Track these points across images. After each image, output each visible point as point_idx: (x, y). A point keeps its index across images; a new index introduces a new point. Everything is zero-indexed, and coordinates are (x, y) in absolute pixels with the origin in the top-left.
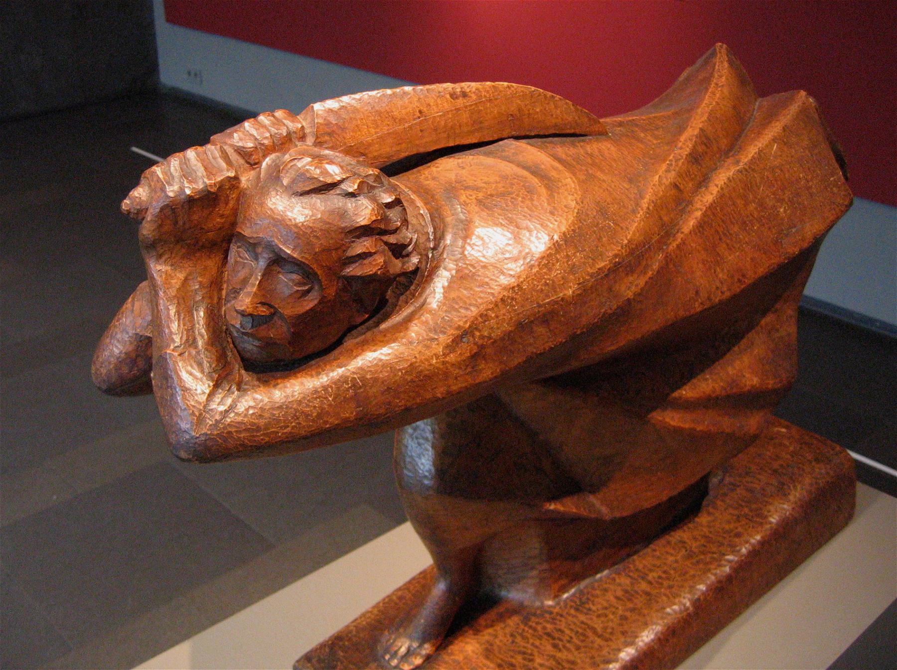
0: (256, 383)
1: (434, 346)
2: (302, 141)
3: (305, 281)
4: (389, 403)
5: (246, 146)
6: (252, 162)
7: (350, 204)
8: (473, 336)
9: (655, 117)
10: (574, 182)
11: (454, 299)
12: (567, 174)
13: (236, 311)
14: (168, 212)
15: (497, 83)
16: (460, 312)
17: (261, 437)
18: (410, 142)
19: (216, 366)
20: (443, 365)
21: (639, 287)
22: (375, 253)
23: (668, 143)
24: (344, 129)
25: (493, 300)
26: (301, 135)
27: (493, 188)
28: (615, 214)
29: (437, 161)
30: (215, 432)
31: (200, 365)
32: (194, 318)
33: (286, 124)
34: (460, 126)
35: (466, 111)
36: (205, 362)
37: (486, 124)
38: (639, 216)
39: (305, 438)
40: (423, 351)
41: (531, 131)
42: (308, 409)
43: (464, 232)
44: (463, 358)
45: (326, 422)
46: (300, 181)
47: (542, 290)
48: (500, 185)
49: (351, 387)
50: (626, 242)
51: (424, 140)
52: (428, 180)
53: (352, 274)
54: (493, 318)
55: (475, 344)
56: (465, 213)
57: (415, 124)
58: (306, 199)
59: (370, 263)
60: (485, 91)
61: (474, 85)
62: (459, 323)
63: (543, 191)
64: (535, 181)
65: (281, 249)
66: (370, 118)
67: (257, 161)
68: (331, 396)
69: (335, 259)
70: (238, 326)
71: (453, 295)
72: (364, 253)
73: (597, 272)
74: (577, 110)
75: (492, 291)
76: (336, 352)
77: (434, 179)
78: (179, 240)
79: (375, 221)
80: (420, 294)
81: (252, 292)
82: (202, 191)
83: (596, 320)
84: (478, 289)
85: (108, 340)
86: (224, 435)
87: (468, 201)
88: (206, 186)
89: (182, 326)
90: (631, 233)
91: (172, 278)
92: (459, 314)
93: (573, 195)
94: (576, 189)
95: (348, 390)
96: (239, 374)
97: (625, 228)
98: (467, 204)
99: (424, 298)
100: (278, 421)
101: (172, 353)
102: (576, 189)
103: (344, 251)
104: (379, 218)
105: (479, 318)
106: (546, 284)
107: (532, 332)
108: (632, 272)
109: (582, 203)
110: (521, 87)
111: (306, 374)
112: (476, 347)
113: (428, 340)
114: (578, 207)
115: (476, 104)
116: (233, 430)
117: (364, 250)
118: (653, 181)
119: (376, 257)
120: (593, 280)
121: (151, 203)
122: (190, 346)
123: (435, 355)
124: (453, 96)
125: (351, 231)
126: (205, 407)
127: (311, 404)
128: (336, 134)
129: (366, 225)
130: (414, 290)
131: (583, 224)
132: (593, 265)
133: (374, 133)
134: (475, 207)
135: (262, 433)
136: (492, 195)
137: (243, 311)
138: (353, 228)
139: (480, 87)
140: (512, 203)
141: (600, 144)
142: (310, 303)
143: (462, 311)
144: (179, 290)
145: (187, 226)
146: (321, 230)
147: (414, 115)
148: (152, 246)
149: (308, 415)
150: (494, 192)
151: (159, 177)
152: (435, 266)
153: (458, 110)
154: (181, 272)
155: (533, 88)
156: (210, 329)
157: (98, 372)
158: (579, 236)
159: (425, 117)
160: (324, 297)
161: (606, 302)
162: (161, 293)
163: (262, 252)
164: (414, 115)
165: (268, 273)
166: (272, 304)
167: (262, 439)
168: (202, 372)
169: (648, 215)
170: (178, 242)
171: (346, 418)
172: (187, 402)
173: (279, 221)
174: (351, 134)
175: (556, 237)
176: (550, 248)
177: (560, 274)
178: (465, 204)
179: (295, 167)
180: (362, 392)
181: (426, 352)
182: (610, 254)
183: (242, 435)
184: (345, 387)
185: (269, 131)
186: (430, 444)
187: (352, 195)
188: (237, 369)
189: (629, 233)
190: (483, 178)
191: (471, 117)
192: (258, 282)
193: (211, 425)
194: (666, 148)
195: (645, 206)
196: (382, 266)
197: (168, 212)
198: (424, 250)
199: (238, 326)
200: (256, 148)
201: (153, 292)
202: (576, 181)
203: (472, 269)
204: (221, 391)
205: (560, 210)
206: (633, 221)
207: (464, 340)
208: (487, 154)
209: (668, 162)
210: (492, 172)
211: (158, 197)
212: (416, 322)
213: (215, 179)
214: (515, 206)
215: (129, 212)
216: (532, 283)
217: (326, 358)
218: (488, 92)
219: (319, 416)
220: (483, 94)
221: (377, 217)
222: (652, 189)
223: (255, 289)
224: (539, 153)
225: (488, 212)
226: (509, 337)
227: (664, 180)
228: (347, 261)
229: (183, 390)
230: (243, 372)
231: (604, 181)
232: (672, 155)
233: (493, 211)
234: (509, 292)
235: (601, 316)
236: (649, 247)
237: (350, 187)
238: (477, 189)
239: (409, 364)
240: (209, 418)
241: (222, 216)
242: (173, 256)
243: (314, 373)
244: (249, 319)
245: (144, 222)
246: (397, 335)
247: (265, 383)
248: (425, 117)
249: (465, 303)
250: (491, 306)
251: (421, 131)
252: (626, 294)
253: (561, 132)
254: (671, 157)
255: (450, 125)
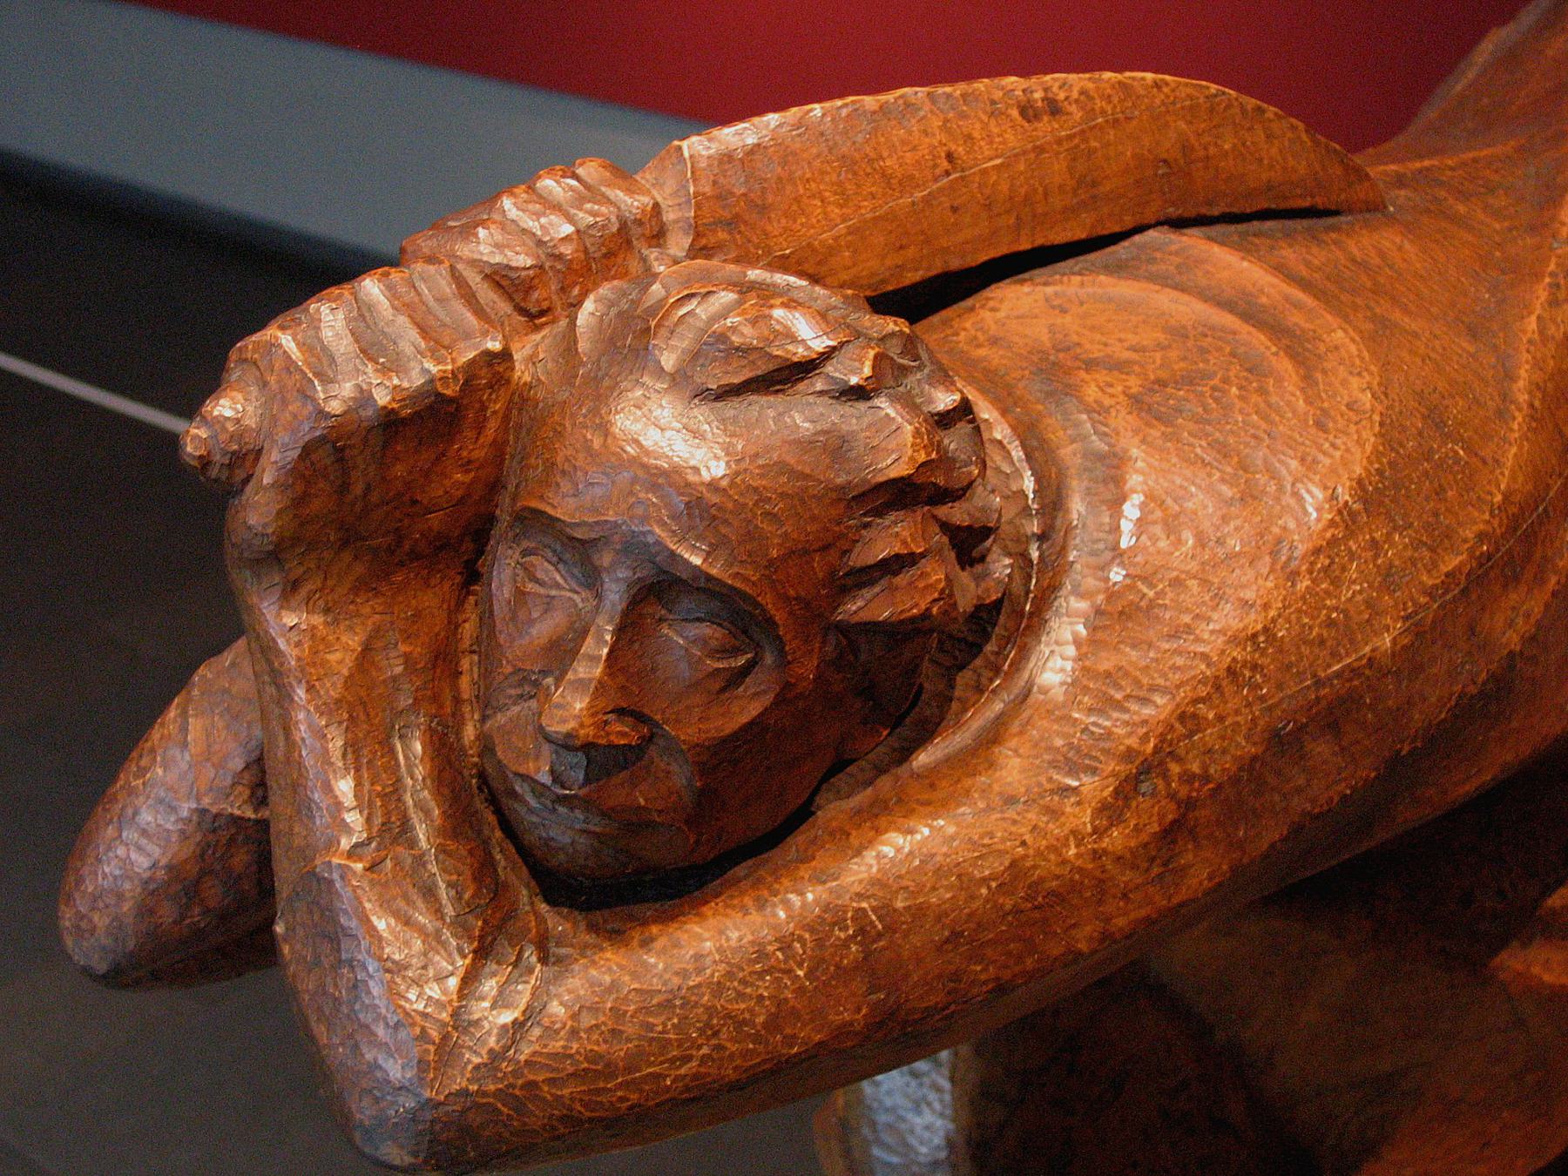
0: (590, 939)
1: (1068, 809)
2: (659, 246)
3: (737, 643)
4: (956, 977)
5: (514, 264)
6: (534, 310)
7: (850, 417)
8: (1165, 775)
9: (1474, 160)
10: (1353, 340)
11: (1108, 674)
12: (1329, 317)
13: (548, 739)
14: (324, 457)
15: (1128, 74)
16: (1127, 710)
17: (619, 1094)
18: (927, 241)
19: (473, 897)
20: (1094, 859)
21: (1532, 621)
22: (923, 555)
23: (1533, 229)
24: (764, 209)
25: (1208, 673)
26: (656, 229)
27: (1159, 362)
28: (1462, 424)
29: (987, 293)
30: (492, 1087)
31: (429, 893)
32: (397, 760)
33: (612, 197)
34: (1046, 195)
35: (1059, 153)
36: (442, 885)
37: (1106, 187)
38: (1516, 427)
39: (735, 1087)
40: (1041, 825)
41: (1209, 203)
42: (743, 1006)
43: (1112, 486)
44: (1144, 837)
45: (790, 1040)
46: (715, 359)
47: (1322, 642)
48: (1173, 354)
49: (854, 937)
50: (1498, 498)
51: (960, 237)
52: (979, 346)
53: (865, 616)
54: (1210, 724)
55: (1172, 796)
56: (1106, 434)
57: (941, 190)
58: (730, 408)
59: (910, 584)
60: (1102, 97)
61: (1078, 81)
62: (1128, 742)
63: (1285, 366)
64: (1257, 341)
65: (673, 554)
66: (827, 179)
67: (545, 305)
68: (800, 965)
69: (821, 575)
70: (545, 778)
71: (1106, 663)
72: (897, 555)
73: (1443, 582)
74: (1316, 142)
75: (1201, 649)
76: (799, 839)
77: (994, 341)
78: (349, 538)
79: (923, 465)
80: (1017, 666)
81: (590, 680)
82: (420, 394)
83: (1443, 716)
84: (1167, 646)
85: (110, 831)
86: (517, 1092)
87: (1107, 402)
88: (432, 381)
89: (367, 786)
90: (1507, 473)
91: (329, 648)
92: (1126, 717)
93: (1359, 374)
94: (1362, 359)
95: (845, 944)
96: (536, 914)
97: (1490, 461)
98: (1107, 411)
99: (1026, 675)
100: (665, 1045)
101: (347, 863)
102: (1362, 359)
103: (845, 552)
104: (934, 456)
105: (1177, 725)
106: (1330, 624)
107: (1302, 758)
108: (1516, 579)
109: (1386, 395)
110: (1186, 85)
111: (727, 906)
112: (1173, 806)
113: (1052, 792)
114: (1380, 408)
115: (1083, 131)
116: (541, 1078)
117: (898, 549)
118: (1524, 332)
119: (926, 565)
120: (1435, 606)
121: (270, 435)
122: (395, 841)
123: (1073, 832)
124: (1028, 111)
125: (863, 494)
126: (455, 1014)
127: (748, 990)
128: (746, 223)
129: (902, 478)
130: (997, 654)
131: (1398, 453)
132: (1435, 565)
133: (838, 221)
134: (1129, 418)
135: (620, 1080)
136: (1162, 383)
137: (569, 735)
138: (867, 487)
139: (1090, 85)
140: (1216, 400)
141: (1376, 236)
142: (747, 707)
143: (1134, 707)
144: (349, 682)
145: (375, 497)
146: (783, 495)
147: (935, 166)
148: (274, 556)
149: (744, 1022)
150: (1163, 374)
151: (289, 357)
152: (1048, 587)
153: (1040, 150)
154: (351, 628)
155: (1214, 88)
156: (446, 791)
157: (83, 925)
158: (1395, 486)
159: (963, 170)
160: (787, 686)
161: (1463, 664)
162: (301, 693)
163: (613, 563)
164: (935, 166)
165: (630, 627)
166: (646, 711)
167: (621, 1099)
168: (438, 912)
169: (1534, 424)
170: (345, 543)
171: (845, 1024)
172: (403, 1003)
173: (663, 473)
174: (783, 221)
175: (1344, 495)
176: (1332, 523)
177: (1360, 592)
178: (1098, 411)
179: (691, 320)
180: (884, 949)
181: (1051, 826)
182: (1469, 534)
183: (566, 1092)
184: (839, 938)
185: (571, 220)
186: (946, 1072)
187: (859, 393)
188: (526, 899)
189: (1502, 474)
190: (1122, 336)
191: (1071, 169)
192: (606, 651)
193: (477, 1067)
194: (1529, 241)
195: (1523, 398)
196: (942, 591)
197: (324, 457)
198: (1018, 541)
199: (545, 778)
200: (541, 267)
201: (272, 690)
202: (1357, 338)
203: (1145, 590)
204: (494, 967)
205: (1339, 417)
206: (1504, 439)
207: (1144, 788)
208: (1118, 269)
209: (1547, 280)
210: (1141, 318)
211: (295, 416)
212: (1013, 743)
213: (453, 361)
214: (1227, 409)
215: (205, 462)
216: (1299, 619)
217: (775, 855)
218: (1109, 99)
219: (773, 1024)
220: (1099, 104)
221: (928, 454)
222: (1528, 351)
223: (598, 671)
224: (1245, 264)
225: (1163, 428)
226: (1251, 772)
227: (1552, 330)
228: (849, 582)
229: (388, 971)
230: (543, 907)
231: (1416, 335)
232: (1554, 260)
233: (1173, 426)
234: (1245, 649)
235: (1453, 703)
236: (1545, 510)
237: (853, 372)
238: (1120, 367)
239: (1007, 863)
240: (470, 1048)
241: (466, 465)
242: (330, 583)
243: (748, 901)
244: (580, 758)
245: (249, 489)
246: (968, 782)
247: (616, 936)
248: (963, 170)
249: (1137, 682)
250: (1203, 691)
251: (954, 209)
252: (1504, 640)
253: (1284, 205)
254: (1552, 267)
255: (1023, 191)
